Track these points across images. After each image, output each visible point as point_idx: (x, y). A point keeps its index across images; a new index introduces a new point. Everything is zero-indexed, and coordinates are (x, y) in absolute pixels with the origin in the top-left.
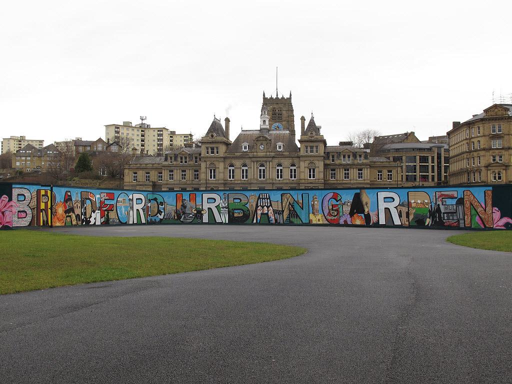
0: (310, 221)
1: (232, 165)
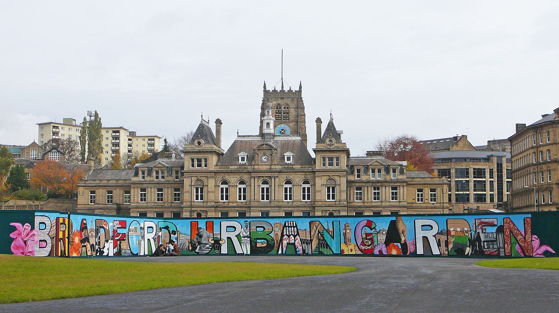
0: (342, 251)
1: (225, 183)
